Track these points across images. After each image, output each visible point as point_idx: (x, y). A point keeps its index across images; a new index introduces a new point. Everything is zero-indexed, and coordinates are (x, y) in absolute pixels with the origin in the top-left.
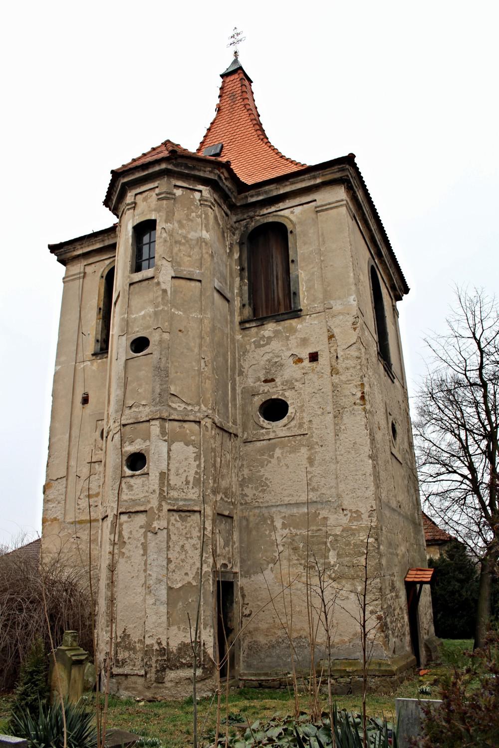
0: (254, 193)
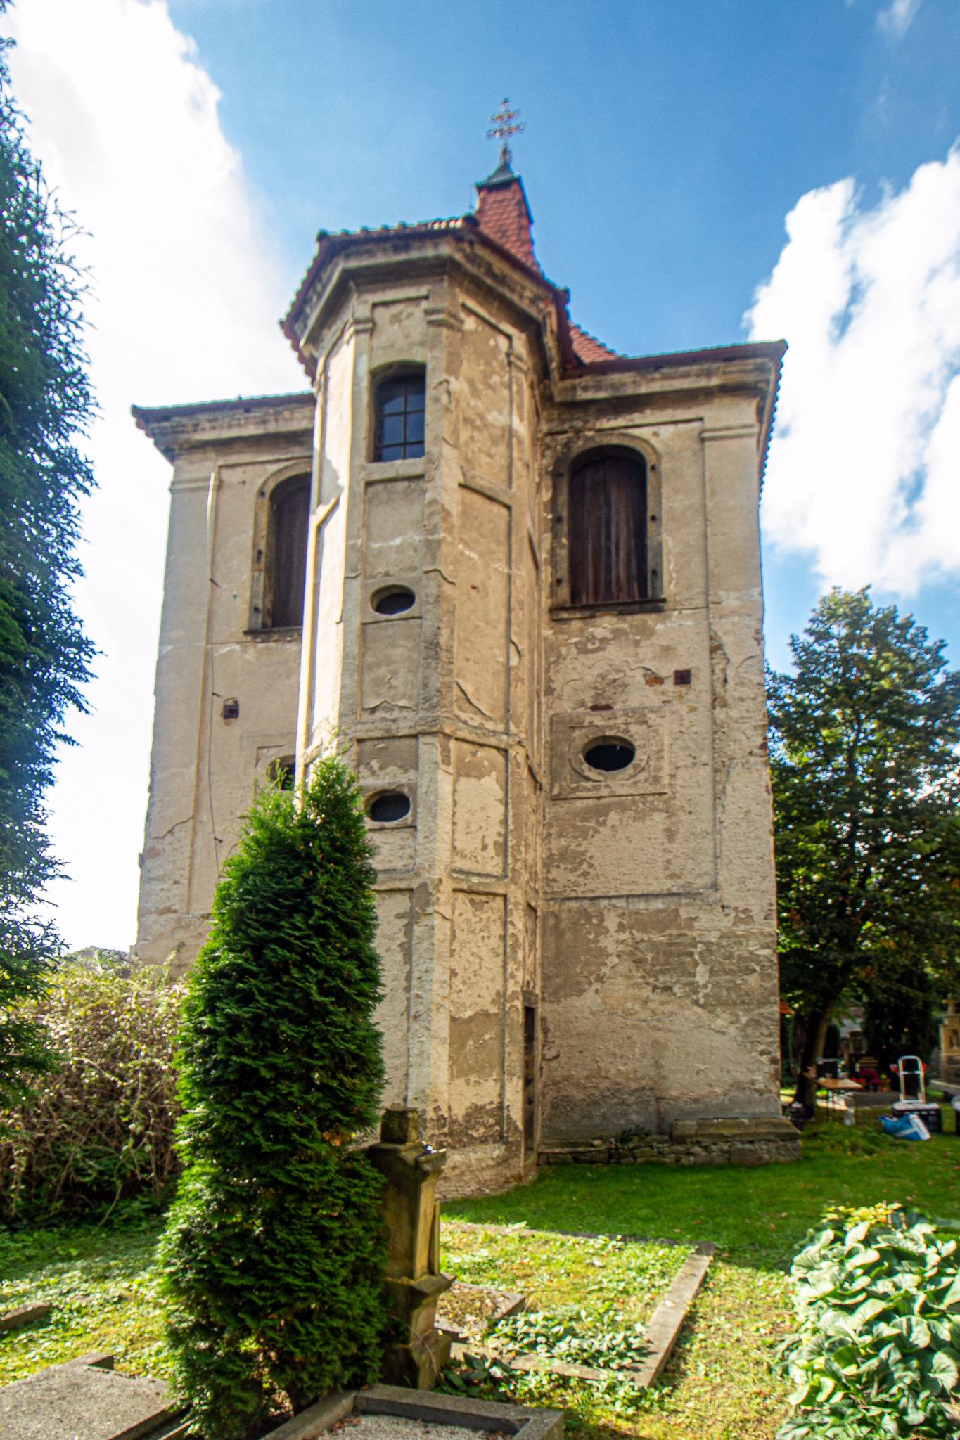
0: (591, 383)
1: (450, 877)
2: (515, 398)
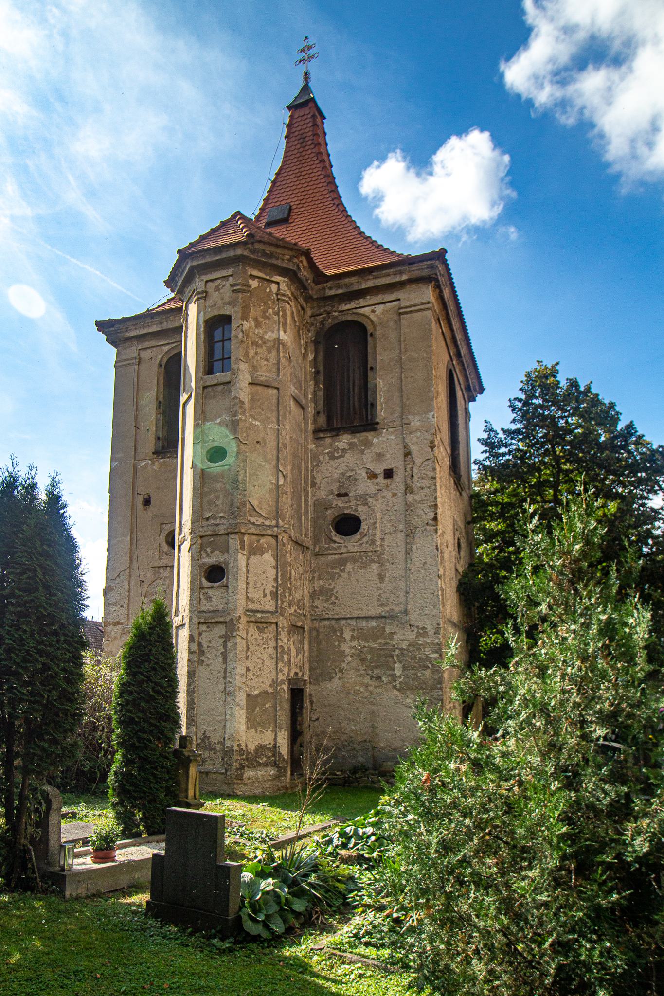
1: (245, 614)
2: (281, 319)
